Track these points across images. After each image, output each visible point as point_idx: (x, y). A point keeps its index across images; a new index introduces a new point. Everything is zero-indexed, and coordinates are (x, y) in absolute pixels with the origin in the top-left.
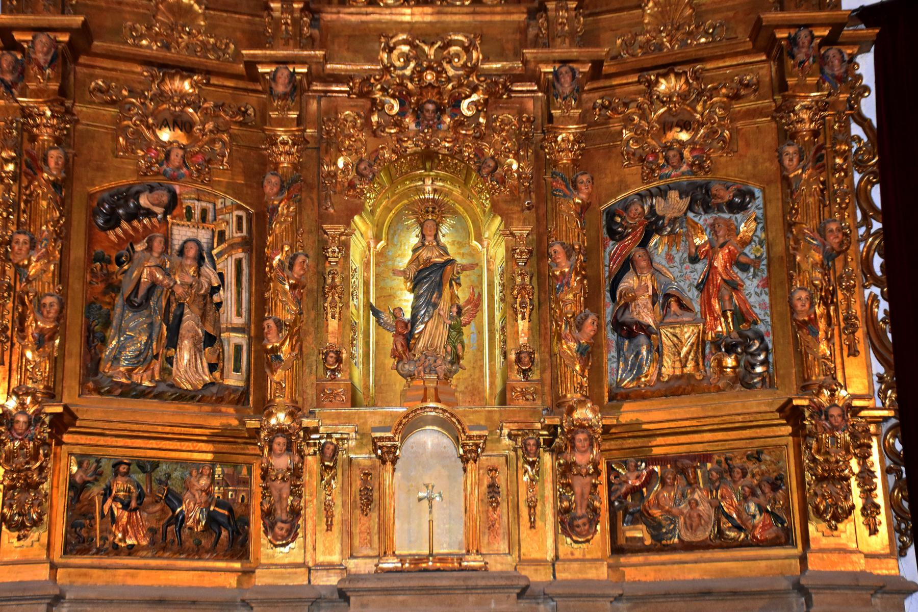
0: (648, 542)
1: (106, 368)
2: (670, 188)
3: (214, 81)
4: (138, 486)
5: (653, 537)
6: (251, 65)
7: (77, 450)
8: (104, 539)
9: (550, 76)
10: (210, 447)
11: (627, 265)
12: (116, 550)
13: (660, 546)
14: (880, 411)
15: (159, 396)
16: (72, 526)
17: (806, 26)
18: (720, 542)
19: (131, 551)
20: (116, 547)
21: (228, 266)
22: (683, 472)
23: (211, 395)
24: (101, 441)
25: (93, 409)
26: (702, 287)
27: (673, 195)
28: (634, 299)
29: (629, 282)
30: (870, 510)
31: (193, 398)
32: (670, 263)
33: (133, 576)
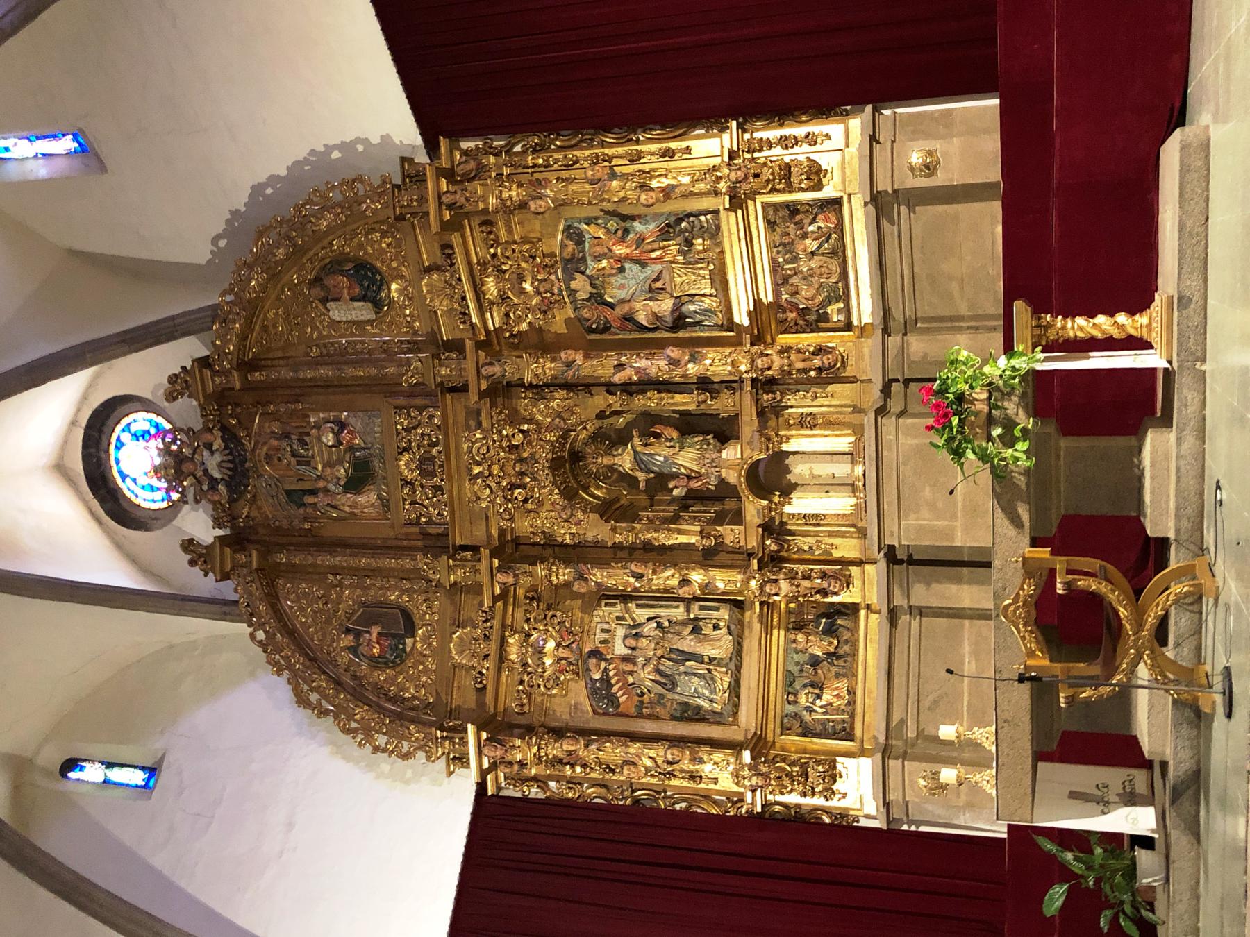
0: (841, 305)
1: (717, 707)
2: (568, 288)
3: (509, 621)
4: (805, 686)
5: (837, 301)
6: (495, 599)
7: (778, 731)
8: (843, 712)
9: (484, 735)
10: (775, 632)
11: (629, 319)
12: (851, 703)
13: (846, 297)
14: (729, 138)
15: (739, 668)
16: (834, 735)
17: (440, 198)
18: (839, 252)
19: (851, 692)
20: (849, 703)
21: (642, 614)
22: (786, 280)
23: (738, 632)
24: (771, 714)
25: (748, 717)
26: (642, 263)
27: (573, 285)
28: (654, 314)
29: (642, 318)
30: (811, 140)
31: (739, 644)
32: (626, 288)
33: (870, 692)
